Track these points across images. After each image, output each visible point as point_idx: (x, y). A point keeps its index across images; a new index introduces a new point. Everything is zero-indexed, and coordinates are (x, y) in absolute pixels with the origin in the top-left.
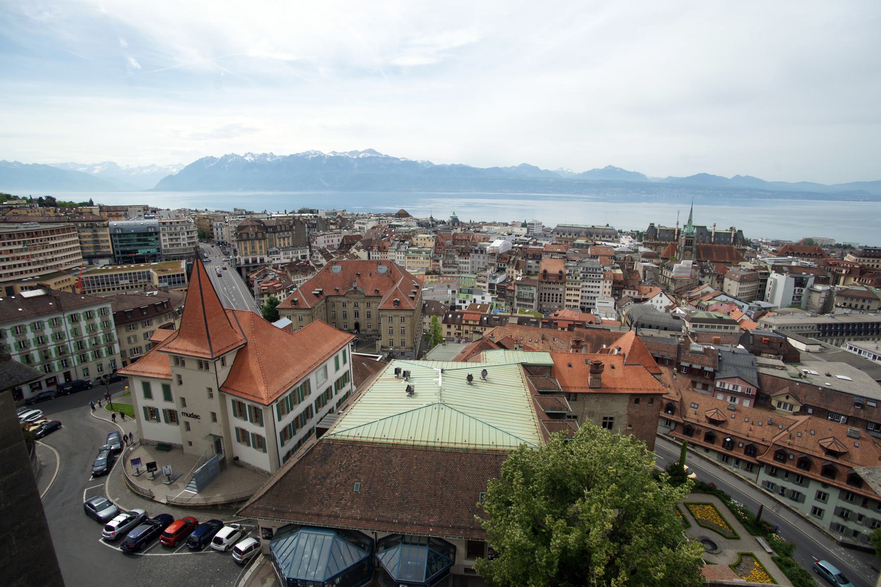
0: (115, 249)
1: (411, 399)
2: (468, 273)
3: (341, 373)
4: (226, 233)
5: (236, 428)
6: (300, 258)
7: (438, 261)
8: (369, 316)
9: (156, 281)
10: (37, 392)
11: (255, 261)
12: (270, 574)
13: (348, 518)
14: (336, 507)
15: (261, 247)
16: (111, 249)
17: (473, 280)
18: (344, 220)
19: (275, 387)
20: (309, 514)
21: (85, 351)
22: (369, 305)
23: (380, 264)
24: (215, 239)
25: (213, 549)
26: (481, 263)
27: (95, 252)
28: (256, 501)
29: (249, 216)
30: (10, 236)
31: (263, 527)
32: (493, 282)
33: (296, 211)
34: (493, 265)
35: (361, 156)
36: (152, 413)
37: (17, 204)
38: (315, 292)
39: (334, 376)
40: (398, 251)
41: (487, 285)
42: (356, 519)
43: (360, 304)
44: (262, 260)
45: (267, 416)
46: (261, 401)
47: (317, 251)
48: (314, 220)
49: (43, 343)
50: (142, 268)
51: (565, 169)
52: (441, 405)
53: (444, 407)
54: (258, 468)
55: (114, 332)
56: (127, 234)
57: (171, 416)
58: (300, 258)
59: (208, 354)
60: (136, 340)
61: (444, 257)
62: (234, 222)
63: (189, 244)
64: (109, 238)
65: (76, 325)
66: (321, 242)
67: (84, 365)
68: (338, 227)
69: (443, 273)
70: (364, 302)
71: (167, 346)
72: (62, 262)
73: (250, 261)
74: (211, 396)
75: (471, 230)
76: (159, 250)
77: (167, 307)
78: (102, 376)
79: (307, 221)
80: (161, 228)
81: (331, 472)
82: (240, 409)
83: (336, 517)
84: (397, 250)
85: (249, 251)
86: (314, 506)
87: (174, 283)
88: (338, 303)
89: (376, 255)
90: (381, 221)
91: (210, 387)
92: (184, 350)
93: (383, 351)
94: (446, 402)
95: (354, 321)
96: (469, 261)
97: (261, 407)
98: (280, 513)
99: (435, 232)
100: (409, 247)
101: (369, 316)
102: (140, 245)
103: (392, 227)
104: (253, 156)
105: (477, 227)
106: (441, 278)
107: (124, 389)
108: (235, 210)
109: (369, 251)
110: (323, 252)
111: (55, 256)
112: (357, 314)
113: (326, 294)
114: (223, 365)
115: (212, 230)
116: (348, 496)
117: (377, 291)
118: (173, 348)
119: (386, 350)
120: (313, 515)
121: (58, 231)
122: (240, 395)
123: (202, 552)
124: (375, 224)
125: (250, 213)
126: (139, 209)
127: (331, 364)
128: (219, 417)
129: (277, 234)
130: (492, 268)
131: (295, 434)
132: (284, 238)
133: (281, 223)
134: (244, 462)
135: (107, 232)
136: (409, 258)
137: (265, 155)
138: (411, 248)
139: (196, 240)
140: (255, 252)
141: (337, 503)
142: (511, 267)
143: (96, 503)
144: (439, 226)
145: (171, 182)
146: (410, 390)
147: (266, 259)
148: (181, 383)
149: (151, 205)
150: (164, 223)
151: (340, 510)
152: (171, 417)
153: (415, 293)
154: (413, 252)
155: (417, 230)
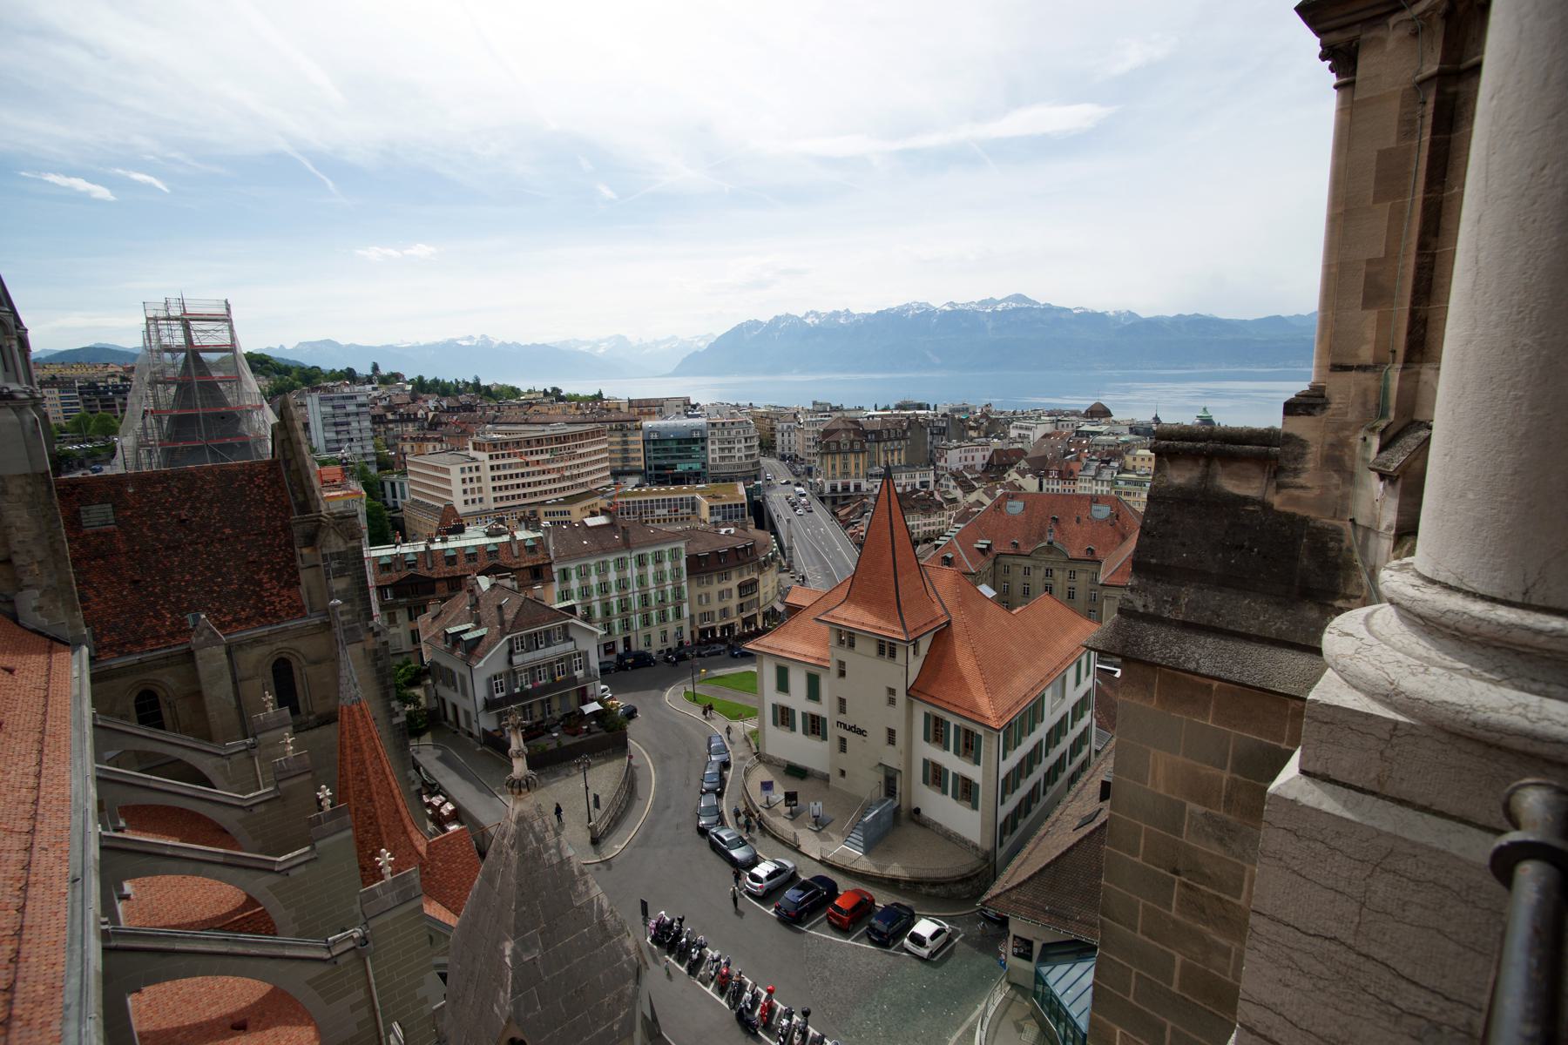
6: (918, 486)
9: (704, 513)
11: (846, 488)
12: (1027, 1018)
15: (857, 466)
16: (642, 463)
18: (993, 422)
21: (666, 606)
23: (1097, 502)
24: (779, 450)
25: (907, 951)
27: (623, 467)
29: (838, 414)
30: (539, 441)
31: (1017, 934)
33: (892, 407)
35: (999, 308)
36: (784, 717)
37: (534, 399)
38: (980, 546)
39: (1074, 695)
40: (1097, 481)
43: (1056, 573)
44: (858, 487)
45: (990, 747)
46: (986, 722)
47: (947, 475)
48: (943, 421)
49: (606, 592)
50: (685, 492)
54: (955, 834)
55: (685, 585)
56: (664, 440)
57: (815, 726)
58: (918, 486)
59: (899, 633)
60: (708, 600)
62: (814, 423)
63: (746, 456)
64: (641, 446)
66: (954, 459)
67: (646, 630)
68: (982, 435)
71: (830, 613)
73: (839, 488)
74: (892, 702)
76: (704, 465)
77: (752, 554)
78: (665, 648)
79: (928, 422)
80: (709, 432)
82: (936, 731)
84: (1094, 478)
89: (1054, 486)
90: (1060, 423)
91: (892, 687)
92: (858, 623)
97: (980, 731)
102: (680, 457)
103: (1082, 436)
104: (817, 315)
107: (700, 672)
108: (815, 403)
110: (957, 476)
111: (582, 471)
113: (995, 550)
115: (773, 435)
118: (840, 619)
121: (587, 435)
123: (891, 951)
124: (1049, 428)
125: (837, 409)
127: (1071, 674)
128: (900, 738)
129: (882, 445)
134: (929, 819)
135: (639, 437)
137: (837, 314)
138: (1124, 475)
139: (756, 451)
145: (695, 363)
148: (842, 674)
150: (714, 425)
152: (813, 727)
154: (1128, 482)
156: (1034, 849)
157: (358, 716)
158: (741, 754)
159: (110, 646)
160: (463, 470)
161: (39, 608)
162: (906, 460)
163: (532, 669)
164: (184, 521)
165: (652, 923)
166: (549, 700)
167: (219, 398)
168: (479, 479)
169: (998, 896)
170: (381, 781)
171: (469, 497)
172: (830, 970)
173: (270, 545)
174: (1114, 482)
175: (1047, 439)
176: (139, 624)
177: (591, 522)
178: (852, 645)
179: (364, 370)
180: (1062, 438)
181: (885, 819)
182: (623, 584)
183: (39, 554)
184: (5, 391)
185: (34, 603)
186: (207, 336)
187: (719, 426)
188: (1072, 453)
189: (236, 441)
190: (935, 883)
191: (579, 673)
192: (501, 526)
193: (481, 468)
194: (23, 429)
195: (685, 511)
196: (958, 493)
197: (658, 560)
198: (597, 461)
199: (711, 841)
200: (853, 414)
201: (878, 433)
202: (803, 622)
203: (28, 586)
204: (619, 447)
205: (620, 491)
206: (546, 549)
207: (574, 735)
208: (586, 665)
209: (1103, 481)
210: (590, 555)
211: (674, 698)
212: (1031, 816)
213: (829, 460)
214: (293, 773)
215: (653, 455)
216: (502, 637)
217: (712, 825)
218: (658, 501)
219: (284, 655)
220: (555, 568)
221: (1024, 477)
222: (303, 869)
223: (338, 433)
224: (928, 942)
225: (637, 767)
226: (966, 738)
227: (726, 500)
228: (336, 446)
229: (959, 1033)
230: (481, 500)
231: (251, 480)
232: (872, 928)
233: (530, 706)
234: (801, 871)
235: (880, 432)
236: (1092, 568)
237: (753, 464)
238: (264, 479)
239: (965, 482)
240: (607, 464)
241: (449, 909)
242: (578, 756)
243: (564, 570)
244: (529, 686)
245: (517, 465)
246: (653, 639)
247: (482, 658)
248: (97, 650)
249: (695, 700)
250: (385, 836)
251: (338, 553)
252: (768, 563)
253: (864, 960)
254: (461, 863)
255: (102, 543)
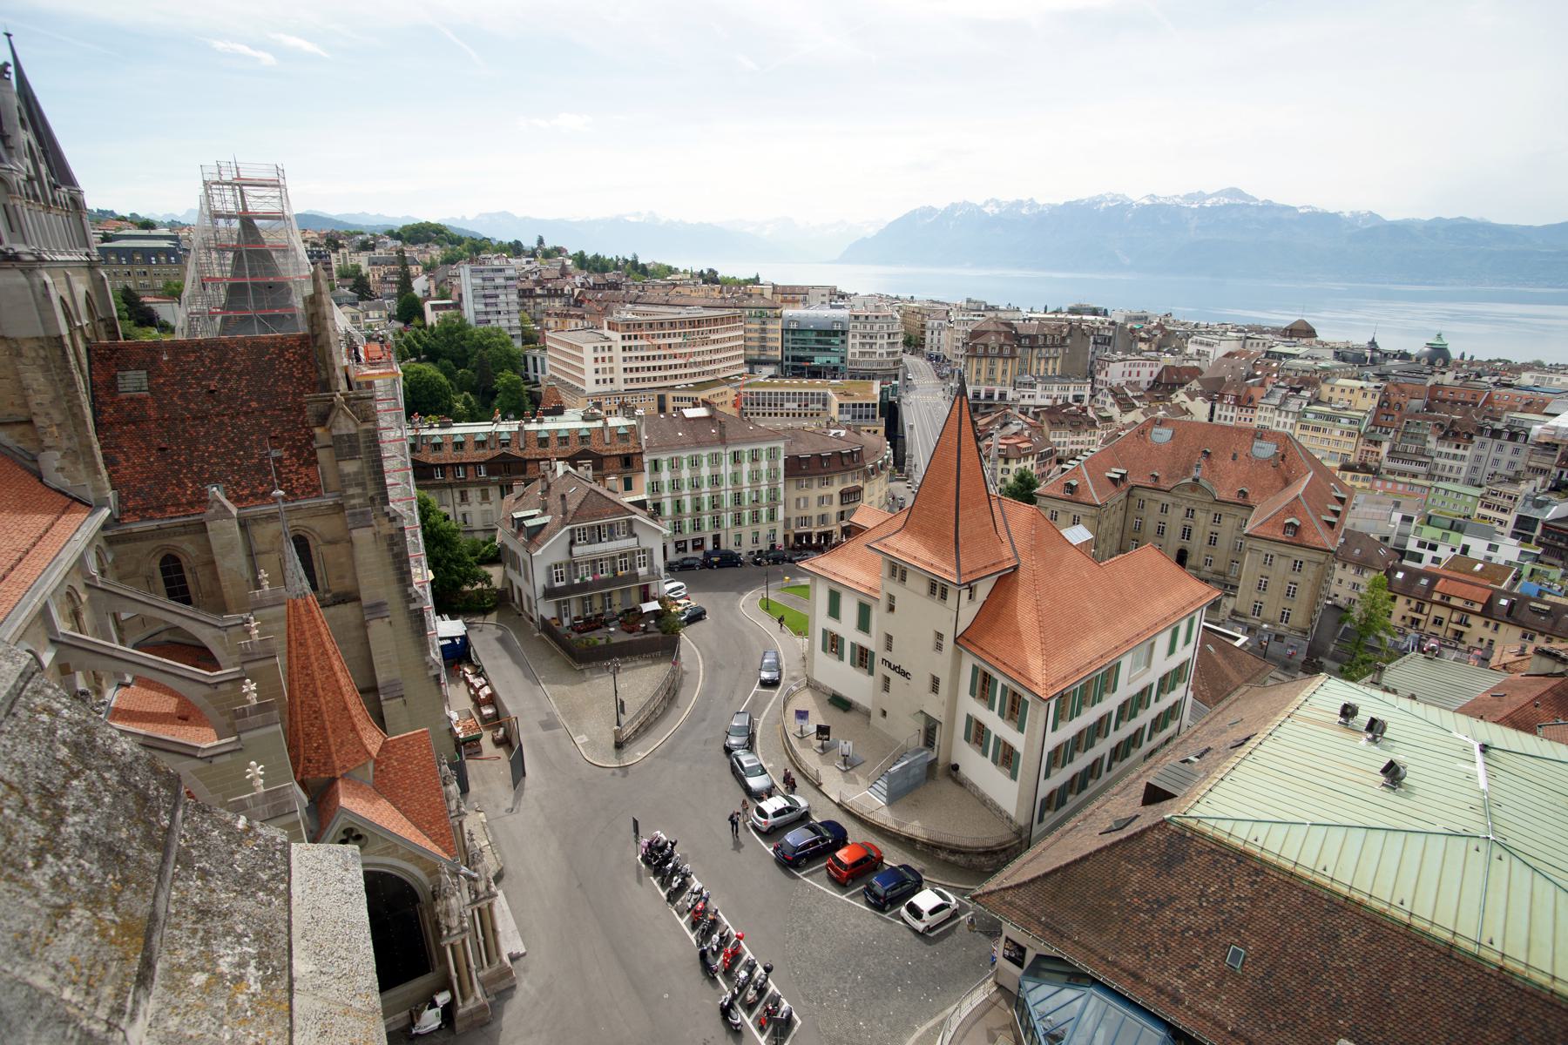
0: (786, 353)
1: (1392, 796)
2: (1456, 480)
3: (1174, 662)
4: (946, 341)
5: (968, 716)
6: (1070, 400)
7: (1377, 443)
8: (1213, 541)
9: (834, 410)
10: (682, 555)
11: (990, 396)
12: (1005, 1028)
13: (1204, 1016)
14: (1179, 977)
15: (1004, 372)
16: (779, 353)
17: (1469, 499)
18: (1168, 335)
19: (1061, 667)
20: (1114, 964)
22: (1217, 518)
23: (1261, 438)
24: (927, 349)
26: (1504, 464)
28: (1011, 887)
29: (992, 314)
30: (672, 324)
32: (1533, 513)
34: (1543, 471)
35: (1208, 204)
36: (833, 643)
39: (1163, 664)
40: (1281, 411)
41: (1511, 519)
42: (1223, 1027)
43: (1198, 514)
44: (1002, 396)
45: (1036, 716)
47: (1105, 391)
48: (1109, 329)
52: (1496, 847)
53: (1506, 856)
55: (781, 486)
57: (863, 658)
58: (1070, 400)
59: (951, 574)
60: (806, 505)
61: (1395, 436)
62: (966, 323)
63: (888, 353)
65: (737, 469)
66: (1115, 373)
67: (738, 530)
68: (1154, 348)
69: (1384, 472)
70: (1208, 511)
71: (884, 541)
72: (721, 366)
73: (982, 396)
74: (939, 647)
75: (1485, 379)
76: (843, 360)
78: (756, 550)
79: (1093, 330)
81: (1177, 898)
82: (983, 686)
83: (1177, 1000)
86: (1129, 952)
87: (860, 417)
88: (1152, 504)
89: (1228, 414)
90: (1249, 341)
92: (910, 556)
93: (1235, 621)
94: (1510, 842)
95: (1178, 545)
96: (1467, 453)
97: (1027, 697)
98: (1053, 931)
99: (1382, 376)
100: (1309, 404)
101: (1213, 541)
104: (998, 204)
105: (1504, 372)
106: (1378, 483)
107: (783, 579)
108: (969, 301)
109: (1213, 402)
110: (1116, 393)
111: (715, 357)
112: (1187, 533)
113: (1131, 481)
114: (970, 597)
115: (923, 333)
116: (1209, 965)
117: (1243, 494)
119: (1243, 620)
120: (1124, 970)
121: (722, 320)
122: (992, 661)
124: (1234, 346)
125: (993, 309)
126: (824, 292)
127: (1163, 641)
129: (1036, 351)
130: (1540, 480)
131: (1071, 760)
132: (1047, 359)
133: (1046, 331)
135: (778, 325)
136: (1303, 427)
137: (1020, 204)
140: (993, 380)
141: (1181, 969)
143: (748, 762)
144: (1389, 363)
145: (861, 251)
146: (1392, 772)
147: (1011, 394)
148: (892, 609)
149: (843, 288)
150: (857, 317)
151: (1186, 988)
152: (861, 659)
153: (1336, 513)
154: (1318, 415)
155: (1334, 367)
156: (1052, 844)
157: (302, 610)
158: (794, 674)
159: (134, 510)
160: (595, 349)
161: (59, 470)
162: (1062, 368)
163: (594, 561)
164: (212, 392)
165: (645, 841)
166: (609, 594)
167: (271, 268)
168: (611, 359)
169: (991, 893)
170: (327, 677)
171: (601, 377)
172: (813, 926)
173: (293, 421)
174: (1301, 415)
175: (1230, 359)
176: (163, 491)
177: (690, 413)
178: (903, 579)
179: (529, 243)
180: (1248, 359)
181: (916, 771)
182: (715, 480)
183: (58, 418)
184: (11, 252)
185: (56, 464)
186: (259, 202)
187: (862, 319)
188: (1256, 376)
189: (287, 313)
190: (955, 851)
191: (642, 571)
192: (597, 411)
193: (614, 348)
194: (33, 292)
195: (816, 406)
196: (1115, 411)
197: (755, 459)
198: (732, 348)
199: (732, 763)
200: (1009, 316)
201: (1033, 339)
202: (855, 546)
203: (50, 448)
204: (757, 335)
205: (752, 380)
206: (638, 437)
207: (630, 632)
208: (651, 564)
209: (1287, 412)
210: (683, 447)
211: (747, 604)
212: (1085, 794)
213: (974, 363)
214: (257, 657)
215: (790, 345)
216: (562, 527)
217: (739, 746)
218: (788, 394)
219: (301, 533)
220: (646, 458)
221: (1193, 400)
222: (228, 758)
223: (486, 305)
224: (926, 916)
225: (686, 673)
226: (1013, 701)
227: (858, 398)
228: (485, 317)
229: (931, 1024)
230: (611, 381)
231: (281, 354)
232: (869, 889)
233: (590, 597)
234: (816, 812)
235: (1036, 337)
236: (1242, 513)
237: (895, 363)
238: (294, 354)
239: (1123, 399)
240: (742, 352)
241: (398, 809)
242: (609, 658)
243: (656, 461)
244: (590, 579)
245: (648, 348)
246: (743, 539)
247: (540, 546)
248: (121, 512)
249: (767, 609)
250: (329, 731)
251: (348, 435)
252: (876, 471)
253: (853, 921)
254: (417, 765)
255: (135, 409)
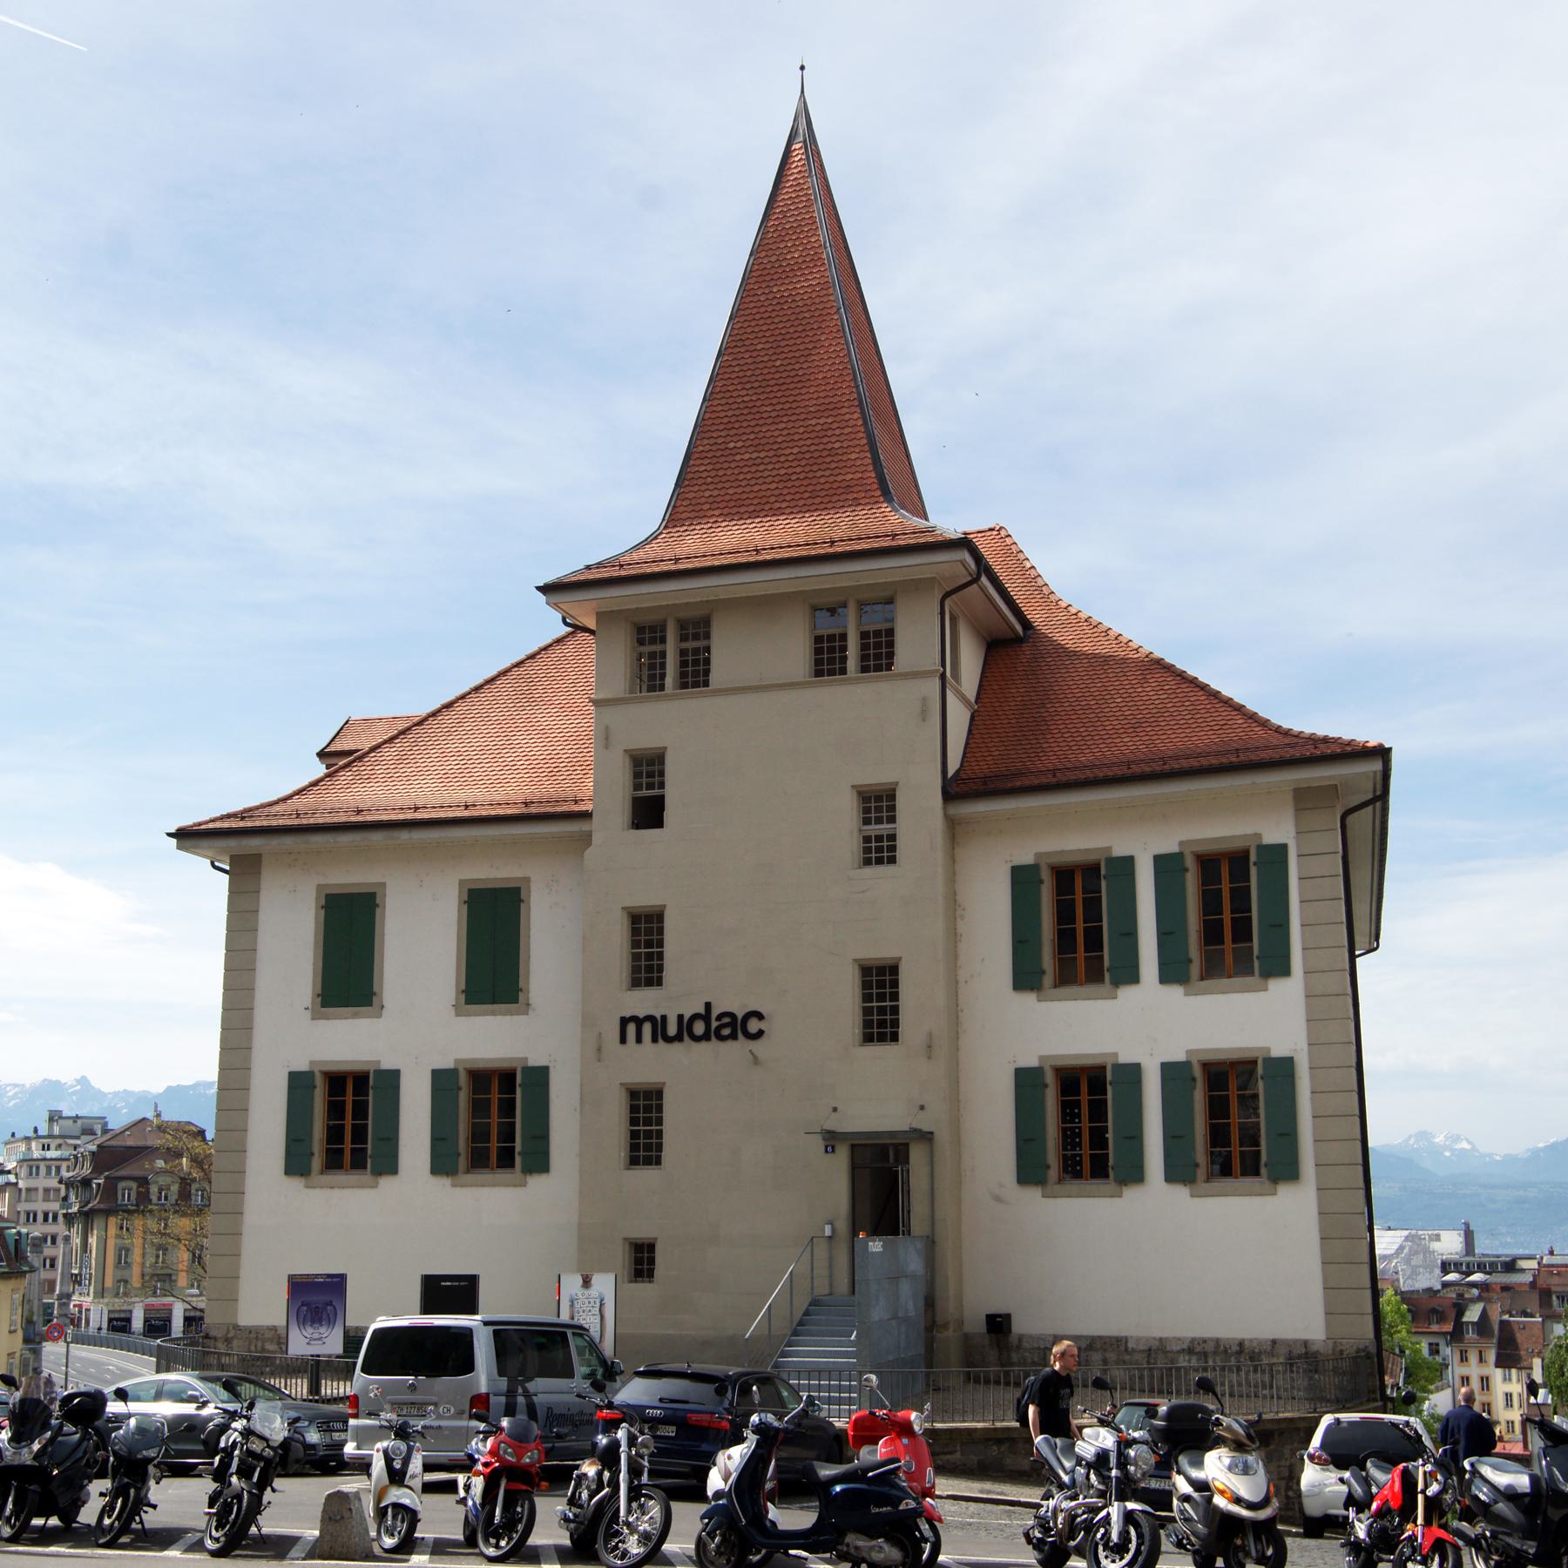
51: (1439, 1139)
85: (136, 1270)
142: (1473, 1357)
